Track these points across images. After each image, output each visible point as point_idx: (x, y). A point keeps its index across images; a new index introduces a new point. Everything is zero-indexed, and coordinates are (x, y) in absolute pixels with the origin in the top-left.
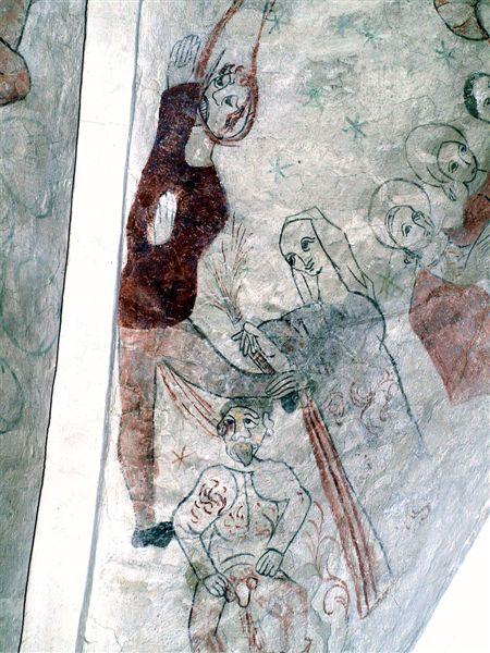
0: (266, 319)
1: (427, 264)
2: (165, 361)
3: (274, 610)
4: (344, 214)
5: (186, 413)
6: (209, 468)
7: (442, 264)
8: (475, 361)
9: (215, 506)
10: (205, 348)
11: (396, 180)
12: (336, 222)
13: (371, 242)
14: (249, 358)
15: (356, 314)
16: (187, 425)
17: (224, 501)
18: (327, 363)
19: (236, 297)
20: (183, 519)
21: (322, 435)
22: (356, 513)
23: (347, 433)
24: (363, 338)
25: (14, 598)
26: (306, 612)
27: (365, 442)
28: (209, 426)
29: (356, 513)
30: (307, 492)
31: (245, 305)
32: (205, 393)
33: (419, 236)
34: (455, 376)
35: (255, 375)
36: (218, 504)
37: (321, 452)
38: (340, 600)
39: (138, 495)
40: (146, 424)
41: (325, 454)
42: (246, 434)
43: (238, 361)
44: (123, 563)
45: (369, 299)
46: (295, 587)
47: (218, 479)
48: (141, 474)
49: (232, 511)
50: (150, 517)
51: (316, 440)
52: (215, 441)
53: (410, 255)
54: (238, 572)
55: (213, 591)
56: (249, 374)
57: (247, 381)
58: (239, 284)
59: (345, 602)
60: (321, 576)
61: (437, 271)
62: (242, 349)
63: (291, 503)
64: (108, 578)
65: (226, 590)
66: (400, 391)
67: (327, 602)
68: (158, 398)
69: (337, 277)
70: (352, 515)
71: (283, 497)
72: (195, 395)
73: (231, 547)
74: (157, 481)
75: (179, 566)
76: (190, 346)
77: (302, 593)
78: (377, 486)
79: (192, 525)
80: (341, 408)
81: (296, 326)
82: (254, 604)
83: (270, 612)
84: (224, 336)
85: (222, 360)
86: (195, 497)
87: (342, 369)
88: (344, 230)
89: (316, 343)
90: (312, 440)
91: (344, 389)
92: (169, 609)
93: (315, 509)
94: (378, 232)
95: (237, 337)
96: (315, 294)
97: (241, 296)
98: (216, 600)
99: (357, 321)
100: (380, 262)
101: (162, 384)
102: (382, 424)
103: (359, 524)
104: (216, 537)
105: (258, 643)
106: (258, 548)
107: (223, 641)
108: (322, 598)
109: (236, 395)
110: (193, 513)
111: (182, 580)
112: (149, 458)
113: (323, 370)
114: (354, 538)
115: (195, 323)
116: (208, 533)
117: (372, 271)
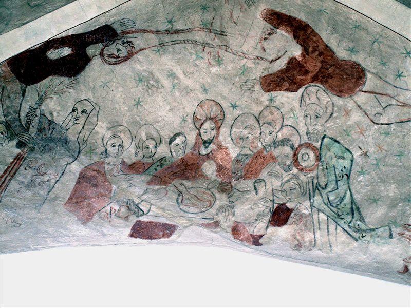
2: (4, 87)
7: (110, 167)
10: (19, 99)
12: (99, 118)
19: (47, 98)
21: (17, 165)
31: (46, 104)
33: (115, 152)
34: (75, 200)
41: (10, 172)
43: (23, 115)
51: (13, 165)
57: (17, 123)
58: (52, 96)
61: (107, 167)
62: (28, 113)
66: (54, 183)
69: (79, 131)
76: (16, 93)
87: (47, 156)
88: (98, 123)
90: (12, 163)
91: (40, 162)
94: (106, 136)
95: (31, 109)
97: (48, 100)
99: (68, 150)
100: (96, 144)
102: (37, 185)
115: (26, 89)
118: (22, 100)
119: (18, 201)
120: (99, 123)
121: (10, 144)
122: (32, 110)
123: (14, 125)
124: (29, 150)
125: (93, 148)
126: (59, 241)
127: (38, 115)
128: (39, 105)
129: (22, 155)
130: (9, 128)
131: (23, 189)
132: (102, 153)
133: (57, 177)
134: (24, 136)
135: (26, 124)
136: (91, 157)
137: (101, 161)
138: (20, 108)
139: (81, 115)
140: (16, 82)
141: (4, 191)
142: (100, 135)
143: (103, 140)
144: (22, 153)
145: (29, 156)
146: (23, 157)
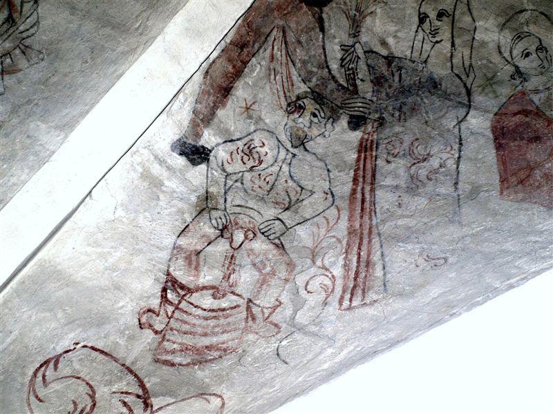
0: (374, 50)
1: (529, 88)
2: (284, 27)
3: (259, 265)
4: (485, 13)
5: (272, 77)
6: (264, 130)
7: (542, 95)
8: (539, 178)
9: (251, 160)
10: (317, 39)
11: (542, 13)
12: (475, 13)
13: (491, 45)
14: (343, 70)
15: (448, 90)
16: (268, 87)
17: (261, 162)
18: (404, 113)
19: (364, 17)
20: (221, 154)
21: (368, 161)
22: (370, 233)
23: (393, 172)
24: (444, 111)
25: (50, 127)
26: (287, 280)
27: (404, 186)
28: (283, 99)
29: (370, 233)
30: (333, 196)
31: (368, 29)
32: (296, 73)
33: (535, 64)
34: (514, 180)
35: (340, 85)
36: (254, 161)
37: (361, 173)
38: (324, 287)
39: (200, 112)
40: (239, 64)
41: (364, 177)
42: (308, 125)
43: (334, 66)
44: (156, 157)
45: (465, 85)
46: (286, 258)
47: (266, 143)
48: (212, 98)
49: (262, 173)
50: (198, 135)
51: (362, 162)
52: (281, 113)
53: (518, 73)
54: (244, 220)
55: (214, 221)
56: (336, 81)
57: (332, 85)
58: (373, 9)
59: (329, 292)
60: (314, 262)
61: (536, 98)
62: (342, 60)
63: (315, 196)
64: (137, 159)
65: (225, 227)
66: (455, 166)
67: (311, 282)
68: (261, 51)
69: (449, 55)
70: (366, 232)
71: (310, 188)
72: (288, 69)
73: (247, 198)
74: (220, 113)
75: (197, 187)
76: (308, 30)
77: (291, 265)
78: (400, 222)
79: (225, 163)
80: (397, 151)
81: (395, 70)
82: (243, 251)
83: (254, 265)
84: (337, 40)
85: (323, 57)
86: (240, 144)
87: (413, 124)
88: (477, 24)
89: (403, 93)
90: (358, 160)
91: (407, 139)
92: (170, 214)
93: (333, 211)
94: (503, 42)
95: (345, 48)
96: (424, 56)
97: (369, 20)
98: (212, 230)
99: (446, 96)
100: (490, 65)
101: (270, 43)
102: (426, 181)
103: (370, 242)
104: (239, 184)
105: (231, 281)
106: (270, 212)
107: (202, 263)
108: (308, 278)
109: (317, 90)
110: (231, 155)
111: (193, 199)
112: (225, 91)
113: (397, 114)
114: (359, 248)
115: (324, 16)
116: (234, 177)
117: (480, 68)
118: (323, 38)
119: (411, 222)
120: (479, 24)
121: (338, 129)
122: (347, 51)
123: (328, 90)
124: (376, 124)
125: (490, 75)
126: (543, 258)
127: (361, 54)
128: (356, 35)
129: (367, 140)
130: (321, 100)
131: (406, 199)
132: (512, 77)
133: (453, 152)
134: (355, 105)
135: (348, 81)
136: (494, 92)
137: (519, 92)
138: (325, 56)
139: (439, 23)
140: (301, 8)
141: (373, 214)
142: (491, 45)
143: (500, 52)
144: (366, 137)
145: (382, 136)
146: (372, 141)
